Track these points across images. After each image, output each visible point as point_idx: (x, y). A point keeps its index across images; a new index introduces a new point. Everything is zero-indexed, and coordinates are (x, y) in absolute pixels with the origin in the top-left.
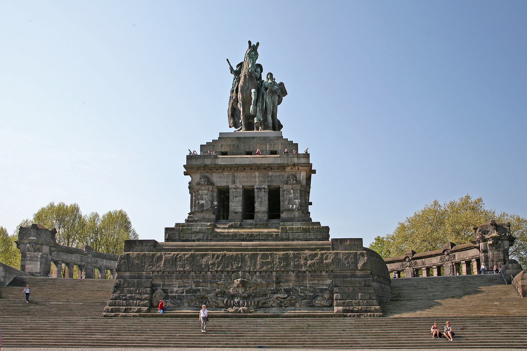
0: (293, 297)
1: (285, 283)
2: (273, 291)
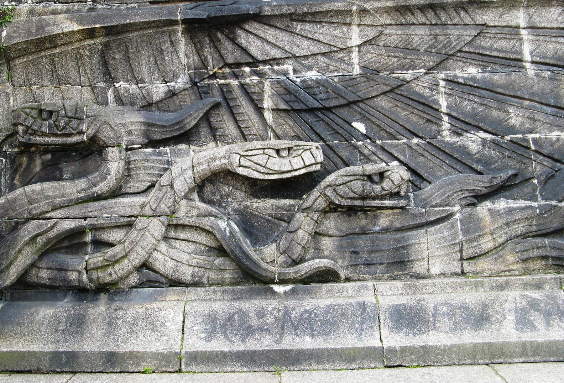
1: (289, 30)
2: (169, 117)
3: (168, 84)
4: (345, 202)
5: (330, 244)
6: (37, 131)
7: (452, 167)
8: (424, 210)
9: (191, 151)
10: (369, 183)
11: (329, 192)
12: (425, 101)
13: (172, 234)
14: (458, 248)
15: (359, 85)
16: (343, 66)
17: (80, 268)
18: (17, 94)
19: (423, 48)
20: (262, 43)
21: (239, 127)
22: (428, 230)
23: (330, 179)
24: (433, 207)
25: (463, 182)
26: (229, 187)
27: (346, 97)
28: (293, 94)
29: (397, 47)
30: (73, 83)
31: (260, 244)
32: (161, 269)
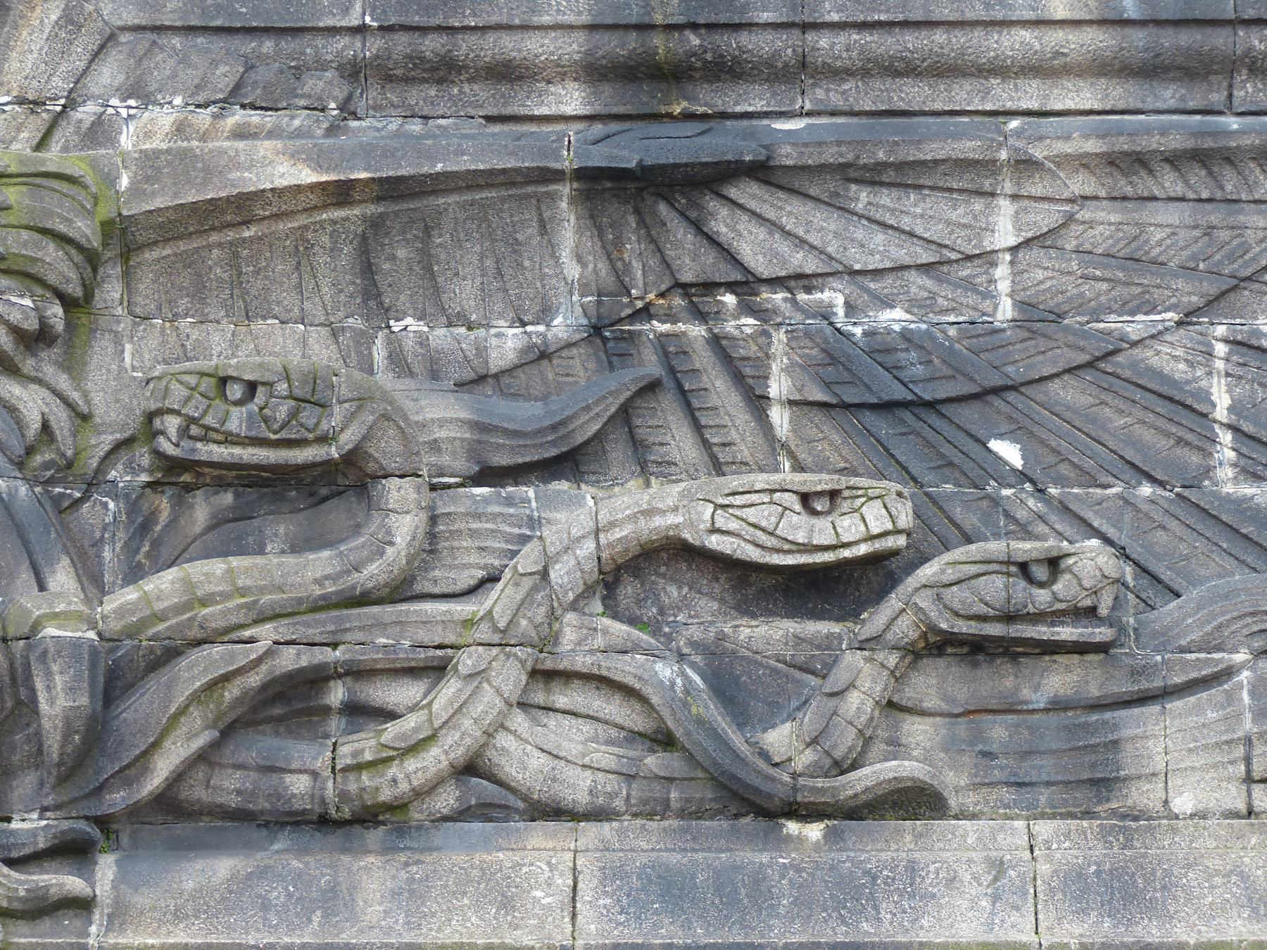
0: (1054, 563)
2: (527, 413)
3: (529, 328)
4: (963, 627)
5: (925, 732)
6: (214, 430)
7: (1237, 559)
8: (1159, 658)
9: (588, 497)
10: (1023, 583)
11: (924, 601)
12: (1175, 392)
13: (539, 698)
14: (1240, 751)
15: (1010, 347)
16: (971, 299)
17: (319, 765)
18: (143, 337)
19: (1176, 260)
20: (771, 233)
21: (706, 444)
22: (1168, 706)
23: (928, 571)
24: (1183, 650)
25: (1258, 594)
26: (680, 588)
27: (976, 377)
28: (843, 365)
29: (1108, 255)
30: (283, 316)
31: (753, 727)
32: (514, 774)
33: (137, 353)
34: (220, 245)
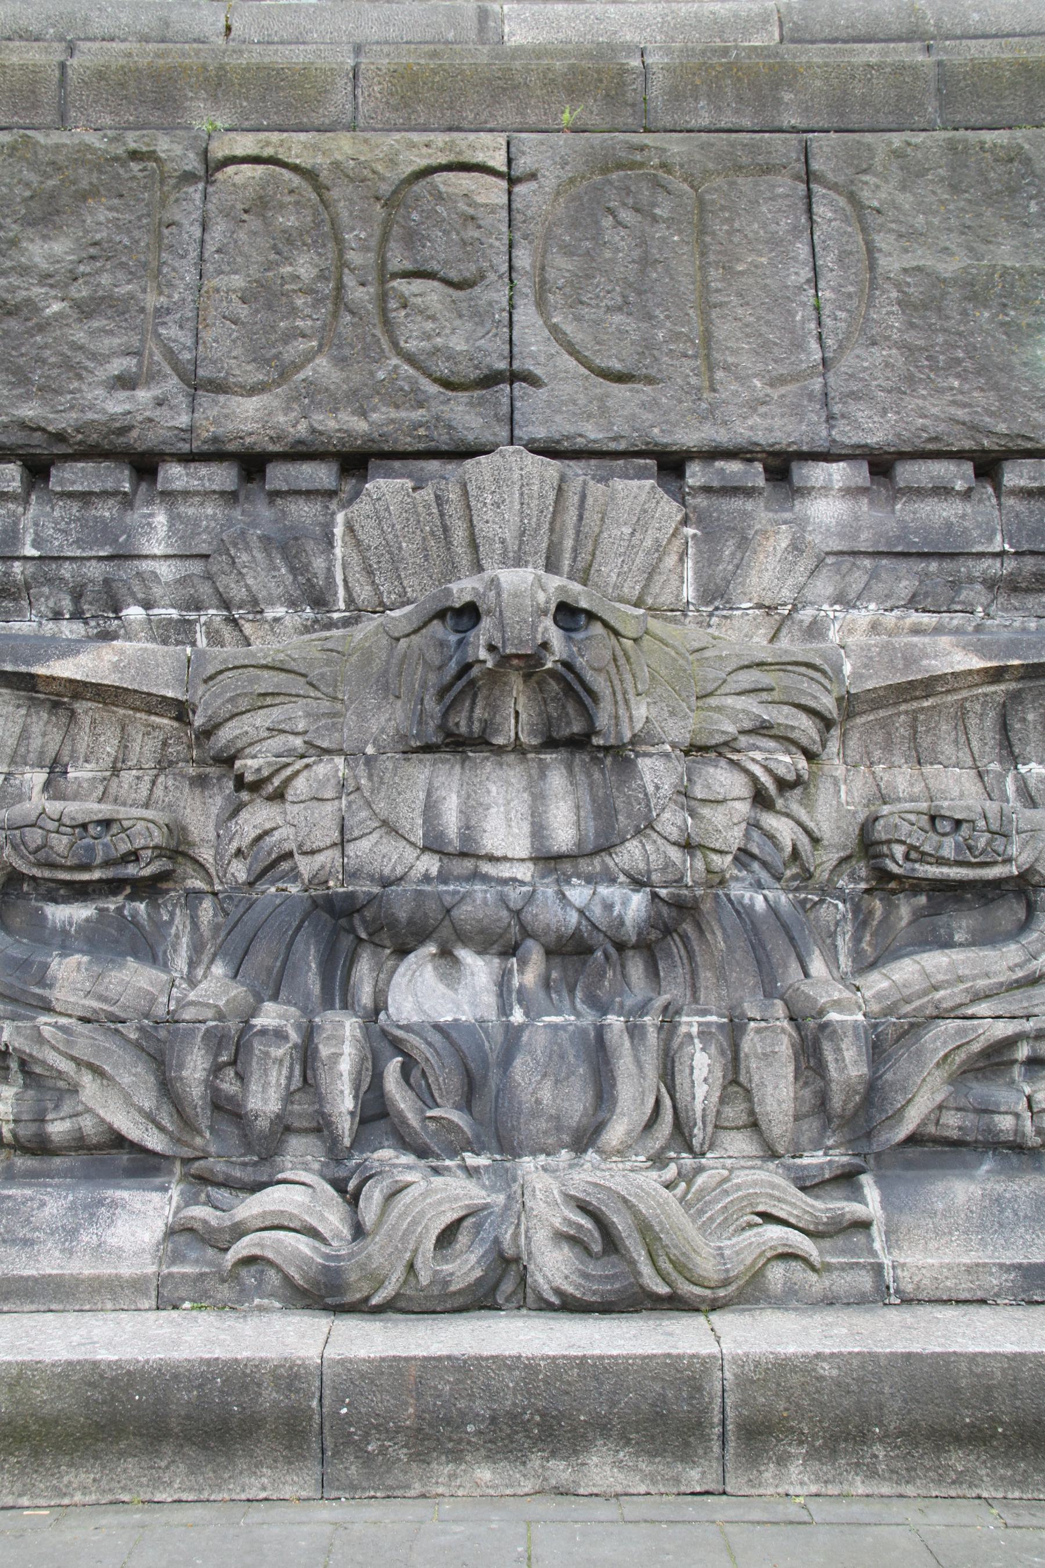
30: (946, 763)
33: (849, 792)
34: (906, 712)
